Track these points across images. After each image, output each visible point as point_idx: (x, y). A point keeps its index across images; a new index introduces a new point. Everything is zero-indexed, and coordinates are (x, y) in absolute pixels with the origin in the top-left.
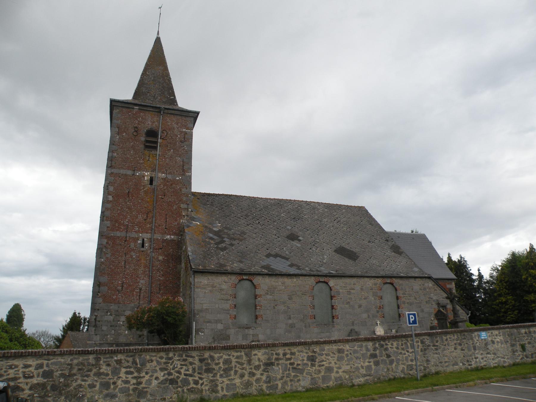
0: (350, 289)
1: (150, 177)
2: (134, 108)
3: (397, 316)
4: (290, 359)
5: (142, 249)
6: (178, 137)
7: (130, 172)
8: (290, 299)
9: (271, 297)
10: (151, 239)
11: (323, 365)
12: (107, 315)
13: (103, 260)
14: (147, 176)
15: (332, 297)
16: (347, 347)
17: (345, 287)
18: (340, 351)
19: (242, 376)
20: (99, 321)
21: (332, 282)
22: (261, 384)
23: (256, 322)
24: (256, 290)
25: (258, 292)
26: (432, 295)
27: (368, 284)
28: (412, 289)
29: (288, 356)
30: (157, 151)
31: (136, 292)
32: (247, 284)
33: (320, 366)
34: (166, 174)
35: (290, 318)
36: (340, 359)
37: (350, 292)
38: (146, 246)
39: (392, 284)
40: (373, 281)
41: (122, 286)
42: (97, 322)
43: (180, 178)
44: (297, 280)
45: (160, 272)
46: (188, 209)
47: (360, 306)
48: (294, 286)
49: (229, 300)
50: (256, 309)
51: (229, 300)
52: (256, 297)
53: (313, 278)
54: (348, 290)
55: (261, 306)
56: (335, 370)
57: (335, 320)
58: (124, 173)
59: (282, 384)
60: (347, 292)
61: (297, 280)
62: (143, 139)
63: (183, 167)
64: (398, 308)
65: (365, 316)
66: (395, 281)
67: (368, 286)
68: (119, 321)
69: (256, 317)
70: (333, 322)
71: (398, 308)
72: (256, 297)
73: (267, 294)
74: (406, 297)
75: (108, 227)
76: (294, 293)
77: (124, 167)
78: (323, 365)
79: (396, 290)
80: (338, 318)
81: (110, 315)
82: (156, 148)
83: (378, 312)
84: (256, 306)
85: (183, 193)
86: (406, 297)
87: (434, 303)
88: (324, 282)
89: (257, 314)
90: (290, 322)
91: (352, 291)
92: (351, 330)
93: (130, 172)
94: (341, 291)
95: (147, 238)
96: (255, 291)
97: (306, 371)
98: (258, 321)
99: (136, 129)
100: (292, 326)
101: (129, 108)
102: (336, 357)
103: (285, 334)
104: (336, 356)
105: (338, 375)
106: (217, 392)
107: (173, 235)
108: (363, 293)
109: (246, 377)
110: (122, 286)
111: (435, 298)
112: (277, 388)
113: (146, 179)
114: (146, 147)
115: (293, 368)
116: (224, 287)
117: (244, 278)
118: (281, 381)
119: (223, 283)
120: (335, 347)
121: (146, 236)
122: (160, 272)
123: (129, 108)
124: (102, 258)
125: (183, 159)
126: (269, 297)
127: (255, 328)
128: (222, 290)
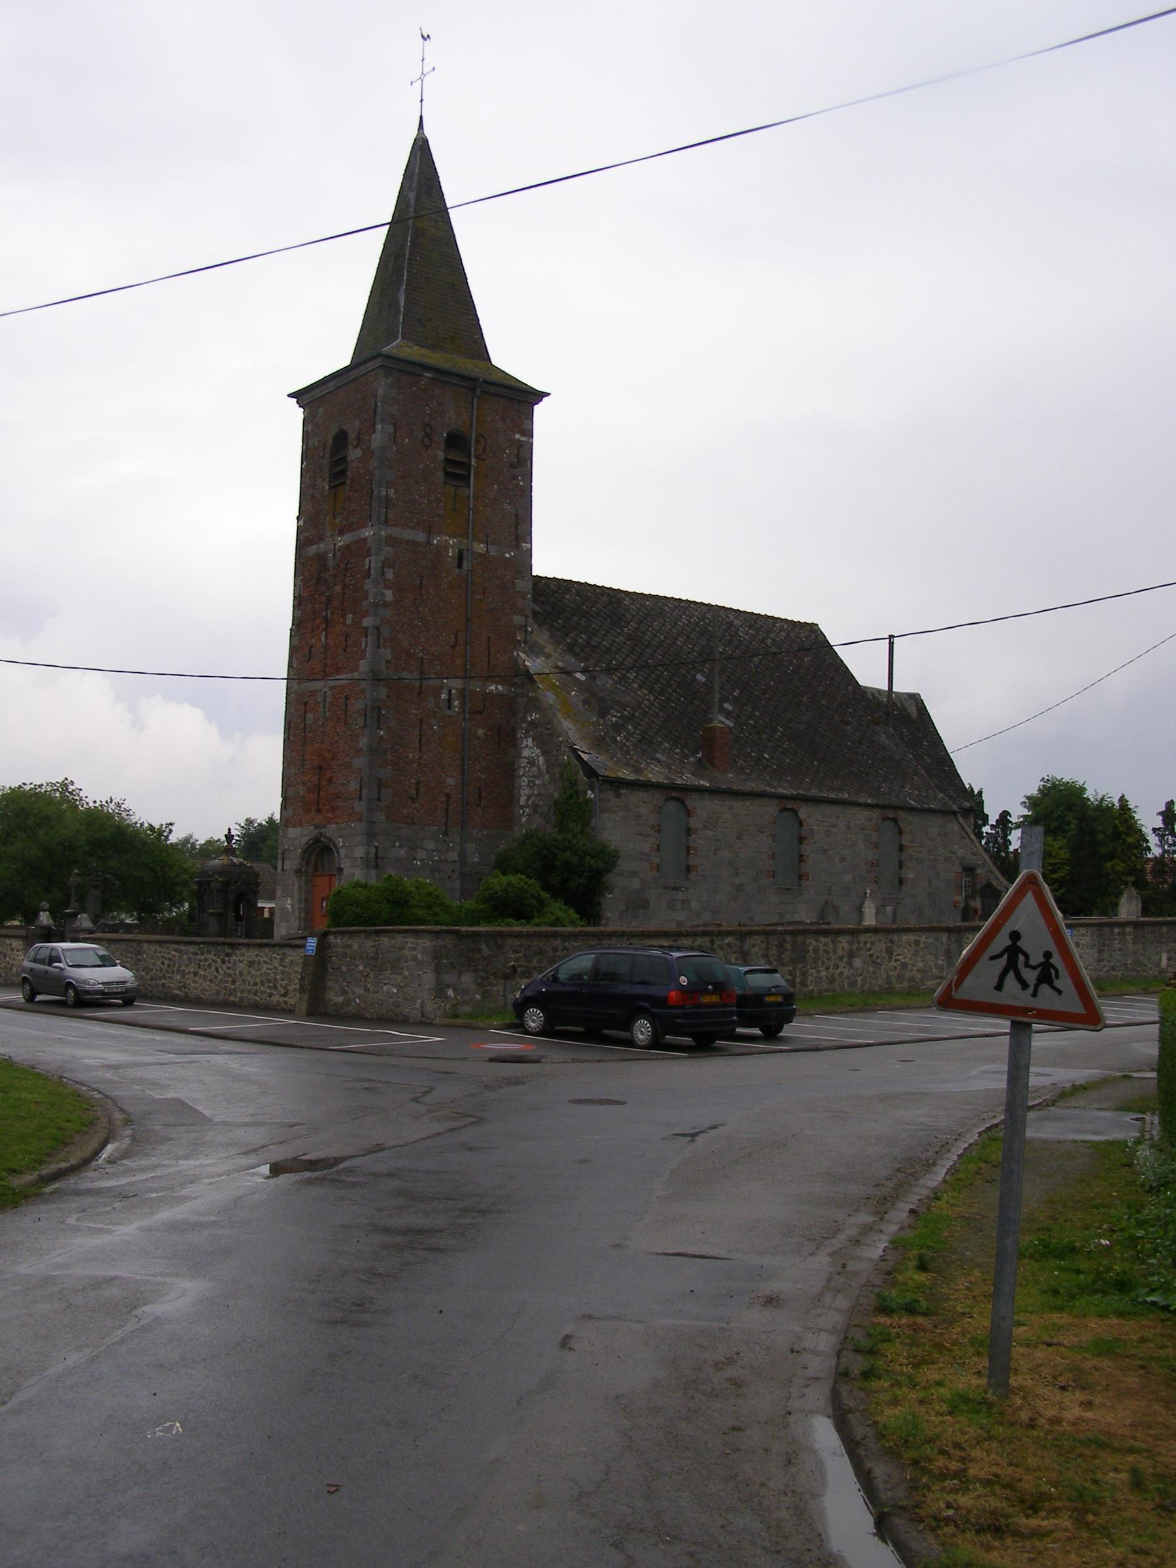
0: (830, 826)
1: (459, 550)
2: (423, 375)
3: (896, 881)
4: (870, 950)
5: (449, 712)
6: (505, 453)
7: (420, 537)
8: (739, 838)
9: (711, 833)
10: (464, 689)
11: (899, 960)
12: (394, 847)
13: (382, 733)
14: (452, 547)
15: (801, 840)
16: (923, 939)
17: (822, 821)
18: (917, 943)
19: (828, 968)
20: (382, 858)
21: (804, 812)
22: (843, 979)
23: (688, 879)
24: (690, 819)
25: (693, 822)
26: (956, 846)
27: (859, 819)
28: (926, 834)
29: (868, 946)
30: (469, 487)
31: (442, 802)
32: (672, 808)
33: (896, 960)
34: (487, 544)
35: (737, 874)
36: (916, 954)
37: (829, 831)
38: (456, 707)
39: (895, 821)
40: (867, 813)
41: (418, 790)
42: (379, 860)
43: (512, 554)
44: (751, 805)
45: (480, 763)
46: (526, 626)
47: (843, 859)
48: (746, 815)
49: (650, 835)
50: (688, 853)
51: (650, 835)
52: (689, 831)
53: (776, 801)
54: (827, 828)
55: (695, 849)
56: (910, 966)
57: (803, 882)
58: (411, 538)
59: (862, 980)
60: (826, 831)
61: (751, 805)
62: (441, 455)
63: (517, 528)
64: (901, 867)
65: (848, 878)
66: (902, 816)
67: (858, 822)
68: (414, 859)
69: (688, 869)
70: (800, 886)
71: (901, 867)
72: (689, 831)
73: (706, 827)
74: (915, 847)
75: (387, 662)
76: (746, 828)
77: (410, 524)
78: (899, 960)
79: (901, 832)
80: (808, 879)
81: (399, 847)
82: (465, 479)
83: (869, 872)
84: (688, 848)
85: (517, 589)
86: (915, 847)
87: (957, 862)
88: (791, 810)
89: (691, 863)
90: (737, 880)
91: (833, 830)
92: (826, 903)
93: (420, 537)
94: (816, 828)
95: (457, 689)
96: (688, 822)
97: (884, 966)
98: (691, 876)
99: (428, 431)
100: (740, 888)
101: (413, 374)
102: (912, 952)
103: (729, 902)
104: (912, 948)
105: (911, 975)
106: (806, 986)
107: (501, 684)
108: (849, 836)
109: (831, 970)
110: (418, 790)
111: (960, 852)
112: (856, 985)
113: (450, 554)
114: (448, 474)
115: (873, 962)
116: (644, 811)
117: (674, 795)
118: (861, 977)
119: (642, 804)
120: (912, 937)
121: (457, 684)
122: (480, 763)
123: (413, 374)
124: (381, 729)
125: (517, 510)
126: (709, 833)
127: (687, 889)
128: (638, 817)
